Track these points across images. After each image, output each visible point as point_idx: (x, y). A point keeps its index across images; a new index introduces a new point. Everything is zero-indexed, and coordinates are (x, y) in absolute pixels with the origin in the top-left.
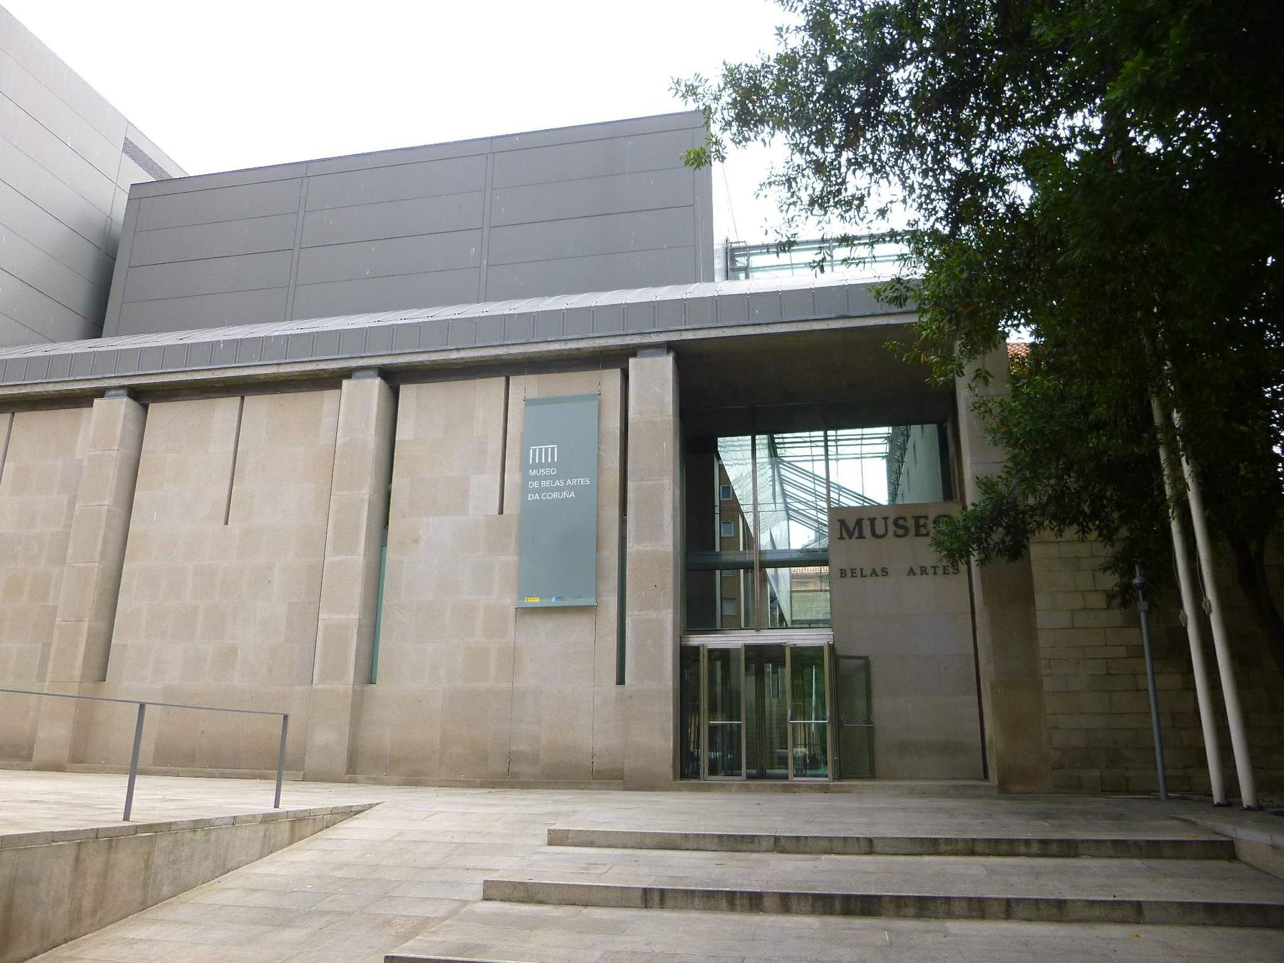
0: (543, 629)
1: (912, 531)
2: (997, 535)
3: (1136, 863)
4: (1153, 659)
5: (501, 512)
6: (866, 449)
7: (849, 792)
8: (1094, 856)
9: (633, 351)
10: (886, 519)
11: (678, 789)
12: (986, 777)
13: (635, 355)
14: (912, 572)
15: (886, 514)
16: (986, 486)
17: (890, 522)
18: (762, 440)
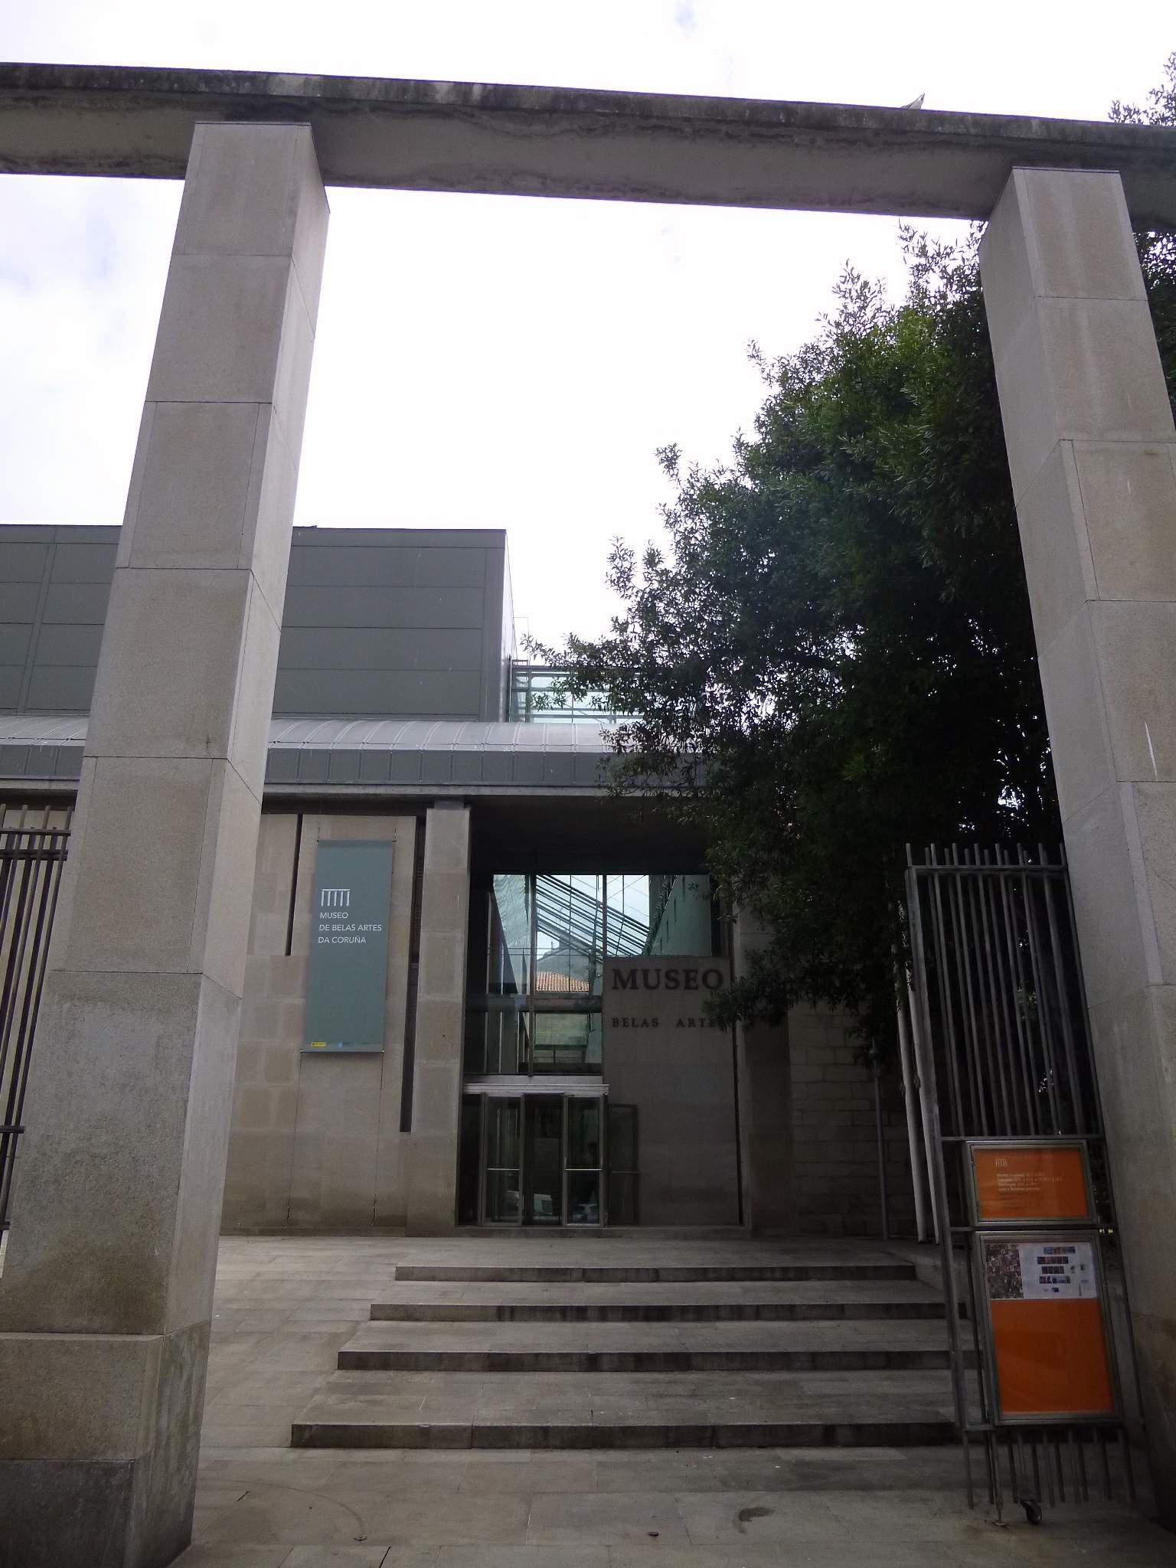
0: (328, 1072)
1: (683, 985)
2: (761, 1005)
3: (848, 1283)
5: (288, 953)
7: (620, 1236)
8: (820, 1279)
9: (430, 802)
11: (459, 1235)
12: (741, 1222)
13: (432, 807)
14: (680, 1023)
16: (754, 958)
17: (662, 974)
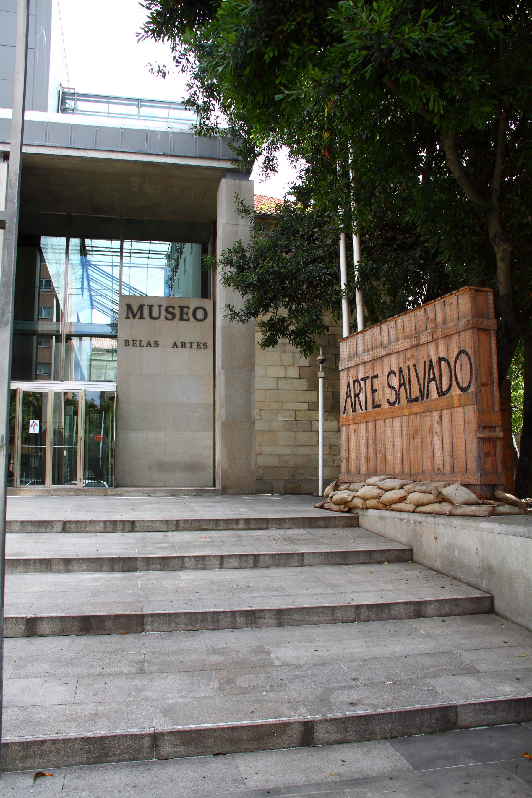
4: (325, 411)
6: (151, 261)
10: (160, 306)
14: (175, 345)
15: (160, 303)
17: (163, 309)
18: (75, 242)
